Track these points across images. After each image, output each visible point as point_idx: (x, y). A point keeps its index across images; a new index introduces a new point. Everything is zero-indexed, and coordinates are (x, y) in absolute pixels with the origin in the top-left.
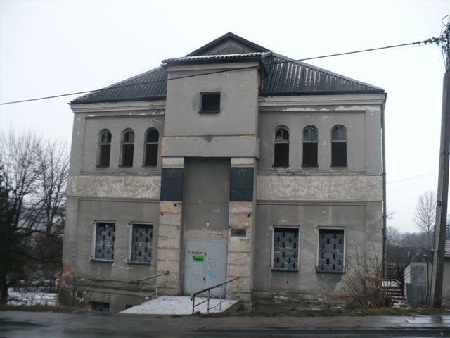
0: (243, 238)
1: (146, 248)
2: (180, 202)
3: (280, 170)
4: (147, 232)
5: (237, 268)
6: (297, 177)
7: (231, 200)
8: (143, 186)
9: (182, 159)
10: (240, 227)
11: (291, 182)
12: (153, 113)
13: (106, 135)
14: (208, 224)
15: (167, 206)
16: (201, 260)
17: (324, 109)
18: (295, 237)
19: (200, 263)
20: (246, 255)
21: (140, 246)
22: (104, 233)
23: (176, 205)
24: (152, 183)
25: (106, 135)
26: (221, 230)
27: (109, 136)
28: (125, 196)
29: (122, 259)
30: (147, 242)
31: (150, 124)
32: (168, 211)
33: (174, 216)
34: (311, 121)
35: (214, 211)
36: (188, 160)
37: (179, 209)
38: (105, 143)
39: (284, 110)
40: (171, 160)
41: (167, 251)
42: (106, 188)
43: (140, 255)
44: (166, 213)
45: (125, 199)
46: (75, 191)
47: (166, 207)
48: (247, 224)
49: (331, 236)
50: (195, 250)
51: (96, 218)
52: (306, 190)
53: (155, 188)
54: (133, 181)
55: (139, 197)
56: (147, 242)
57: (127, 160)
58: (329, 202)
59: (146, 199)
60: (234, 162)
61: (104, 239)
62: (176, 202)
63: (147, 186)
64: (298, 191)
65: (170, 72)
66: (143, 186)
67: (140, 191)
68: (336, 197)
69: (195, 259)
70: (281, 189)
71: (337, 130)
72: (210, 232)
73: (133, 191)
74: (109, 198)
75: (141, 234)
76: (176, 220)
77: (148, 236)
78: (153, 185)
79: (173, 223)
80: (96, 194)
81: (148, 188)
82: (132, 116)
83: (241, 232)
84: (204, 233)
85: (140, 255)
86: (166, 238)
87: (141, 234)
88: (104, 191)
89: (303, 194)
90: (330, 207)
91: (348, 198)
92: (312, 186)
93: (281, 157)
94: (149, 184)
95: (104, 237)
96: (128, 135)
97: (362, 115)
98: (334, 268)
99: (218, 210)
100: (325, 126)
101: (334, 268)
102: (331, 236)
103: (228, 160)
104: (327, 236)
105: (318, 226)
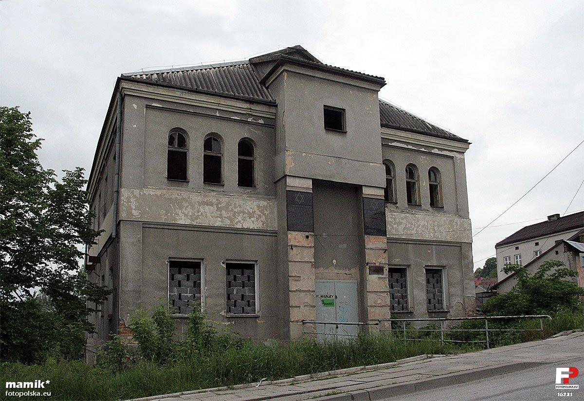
0: (381, 276)
1: (243, 296)
2: (313, 233)
3: (249, 190)
4: (243, 274)
5: (378, 310)
6: (407, 215)
7: (366, 233)
8: (244, 213)
9: (309, 184)
10: (377, 265)
11: (402, 219)
12: (250, 120)
13: (178, 138)
14: (334, 261)
15: (296, 238)
16: (331, 304)
17: (423, 150)
18: (401, 277)
19: (330, 308)
20: (385, 294)
21: (235, 293)
22: (179, 277)
23: (307, 237)
24: (256, 209)
25: (178, 138)
26: (349, 269)
27: (182, 142)
28: (218, 224)
29: (218, 312)
30: (243, 287)
31: (244, 132)
32: (298, 244)
33: (306, 251)
34: (215, 127)
35: (340, 246)
36: (318, 183)
37: (311, 242)
38: (176, 148)
39: (390, 144)
40: (297, 180)
41: (302, 294)
42: (189, 211)
43: (235, 306)
44: (296, 246)
45: (220, 228)
46: (135, 213)
47: (295, 239)
48: (383, 261)
49: (434, 274)
50: (323, 293)
51: (172, 254)
52: (415, 229)
53: (260, 216)
54: (228, 204)
55: (239, 226)
56: (243, 287)
57: (212, 174)
58: (433, 241)
59: (248, 230)
60: (366, 191)
61: (180, 284)
62: (307, 234)
63: (248, 212)
64: (408, 229)
65: (287, 71)
66: (244, 213)
67: (240, 218)
68: (440, 238)
69: (325, 304)
70: (394, 226)
71: (433, 171)
72: (336, 271)
73: (229, 218)
74: (195, 226)
75: (235, 277)
76: (308, 255)
77: (246, 280)
78: (258, 212)
79: (307, 259)
80: (175, 219)
81: (251, 216)
82: (220, 118)
83: (378, 270)
84: (333, 271)
85: (235, 306)
86: (298, 278)
87: (235, 277)
88: (186, 215)
89: (413, 232)
90: (434, 247)
91: (449, 239)
92: (419, 225)
93: (389, 196)
94: (251, 211)
95: (179, 282)
96: (212, 141)
97: (450, 161)
98: (435, 308)
99: (345, 246)
100: (424, 164)
101: (435, 308)
102: (434, 274)
103: (358, 188)
104: (236, 272)
105: (426, 266)
